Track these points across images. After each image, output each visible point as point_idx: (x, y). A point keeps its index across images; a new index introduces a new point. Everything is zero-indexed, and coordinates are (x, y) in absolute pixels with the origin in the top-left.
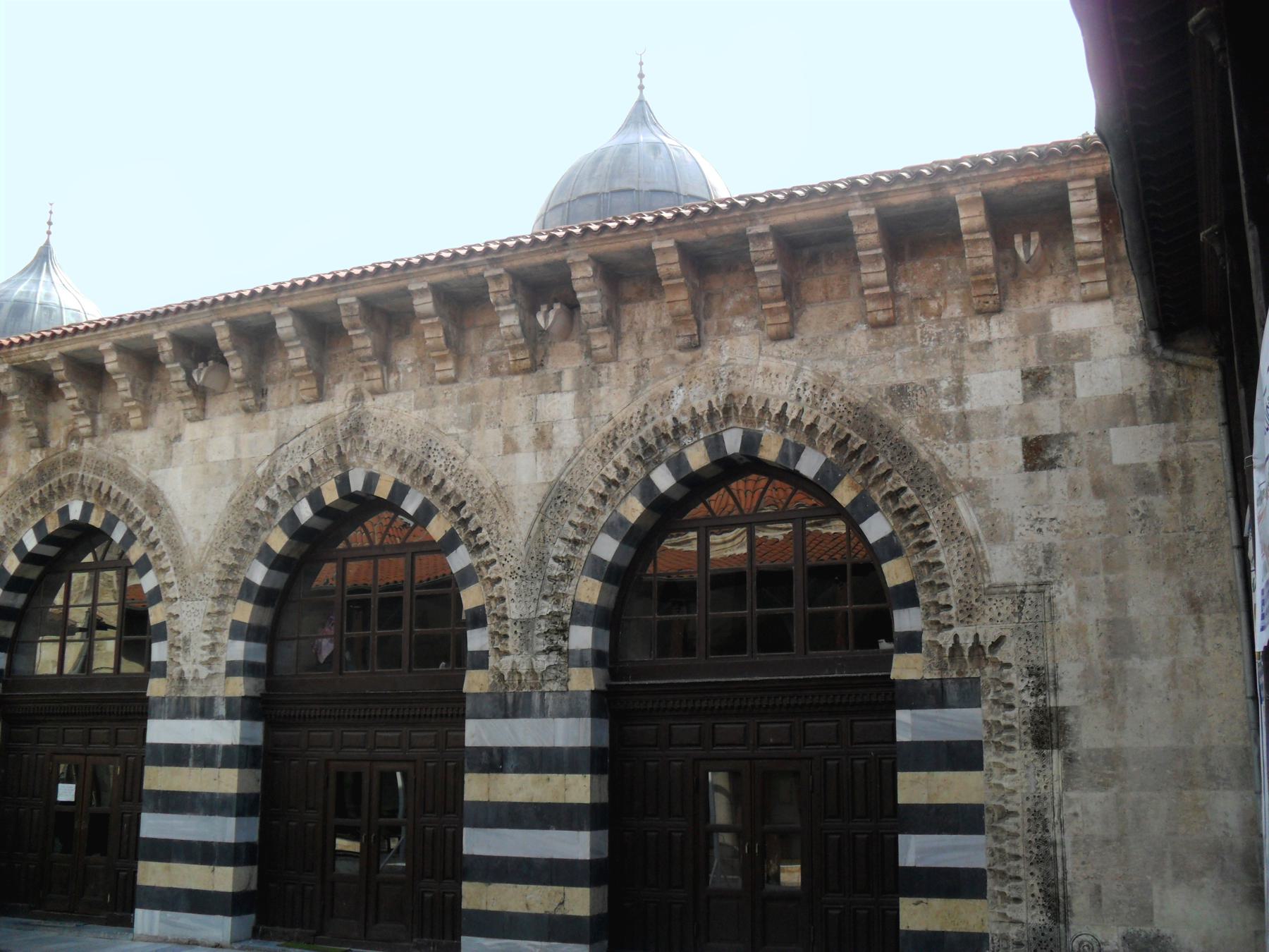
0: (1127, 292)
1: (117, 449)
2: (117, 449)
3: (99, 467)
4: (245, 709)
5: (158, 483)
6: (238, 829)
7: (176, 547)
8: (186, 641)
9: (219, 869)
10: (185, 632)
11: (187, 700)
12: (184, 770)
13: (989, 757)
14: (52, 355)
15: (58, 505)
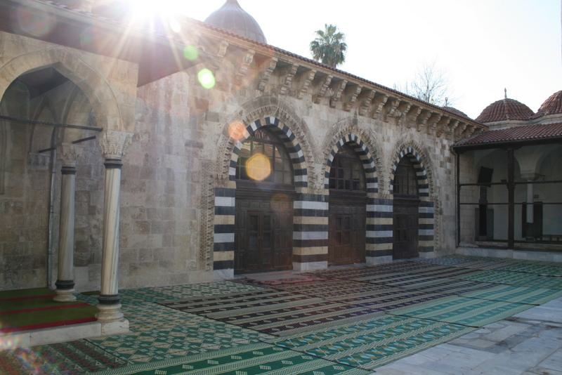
0: (154, 66)
1: (291, 103)
2: (291, 103)
3: (285, 107)
4: (327, 199)
5: (305, 120)
6: (301, 236)
7: (312, 146)
8: (317, 176)
9: (324, 247)
10: (316, 174)
11: (314, 195)
12: (314, 218)
13: (435, 216)
14: (296, 64)
15: (265, 116)
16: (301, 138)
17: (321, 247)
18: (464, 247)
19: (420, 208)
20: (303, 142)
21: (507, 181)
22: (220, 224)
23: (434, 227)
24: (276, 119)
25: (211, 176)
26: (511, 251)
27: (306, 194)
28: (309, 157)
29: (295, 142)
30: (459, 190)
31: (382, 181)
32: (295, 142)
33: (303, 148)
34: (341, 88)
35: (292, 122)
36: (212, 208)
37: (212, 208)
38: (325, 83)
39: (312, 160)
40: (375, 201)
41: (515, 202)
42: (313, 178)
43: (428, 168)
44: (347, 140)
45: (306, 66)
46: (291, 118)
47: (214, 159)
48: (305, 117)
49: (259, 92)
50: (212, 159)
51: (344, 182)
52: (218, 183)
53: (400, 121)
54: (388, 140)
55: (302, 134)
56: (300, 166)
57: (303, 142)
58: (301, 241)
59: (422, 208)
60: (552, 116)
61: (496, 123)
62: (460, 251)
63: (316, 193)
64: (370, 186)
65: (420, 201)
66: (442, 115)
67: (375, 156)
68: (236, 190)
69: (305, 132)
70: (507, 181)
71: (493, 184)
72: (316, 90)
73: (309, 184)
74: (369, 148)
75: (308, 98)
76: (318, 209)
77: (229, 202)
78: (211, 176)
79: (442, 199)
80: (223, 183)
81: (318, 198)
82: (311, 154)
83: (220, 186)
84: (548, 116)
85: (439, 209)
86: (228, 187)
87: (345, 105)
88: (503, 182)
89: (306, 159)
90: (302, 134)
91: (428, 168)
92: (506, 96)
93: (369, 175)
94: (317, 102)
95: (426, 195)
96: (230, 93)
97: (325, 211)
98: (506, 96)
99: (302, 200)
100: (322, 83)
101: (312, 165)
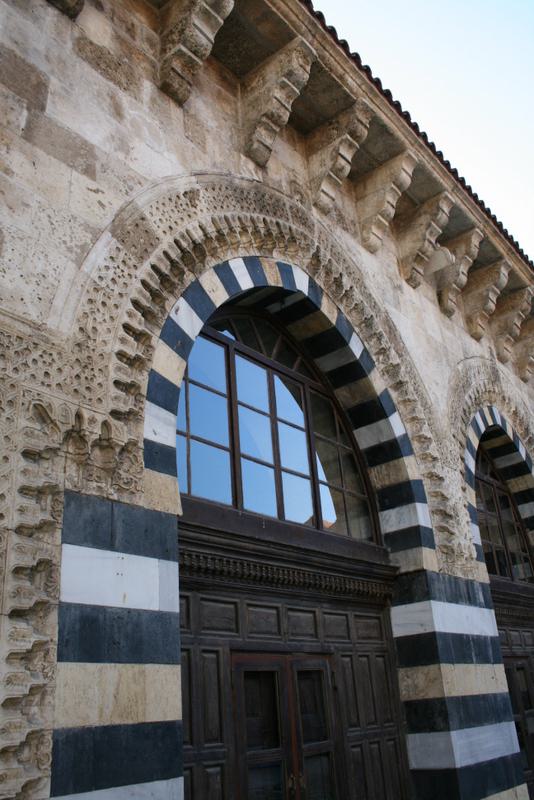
6: (450, 751)
8: (454, 508)
16: (392, 371)
22: (94, 720)
24: (312, 284)
25: (42, 414)
29: (378, 382)
33: (401, 407)
34: (468, 253)
36: (41, 607)
37: (41, 607)
39: (433, 450)
40: (437, 586)
42: (446, 515)
45: (399, 134)
46: (357, 295)
47: (63, 324)
49: (251, 166)
50: (51, 323)
52: (84, 463)
56: (400, 469)
63: (460, 575)
68: (182, 523)
69: (400, 356)
73: (438, 538)
76: (476, 632)
77: (144, 584)
78: (42, 414)
80: (112, 472)
81: (461, 593)
82: (426, 432)
83: (91, 489)
86: (141, 501)
87: (469, 320)
89: (416, 445)
90: (396, 360)
94: (412, 282)
96: (145, 108)
99: (427, 596)
100: (424, 219)
101: (438, 471)
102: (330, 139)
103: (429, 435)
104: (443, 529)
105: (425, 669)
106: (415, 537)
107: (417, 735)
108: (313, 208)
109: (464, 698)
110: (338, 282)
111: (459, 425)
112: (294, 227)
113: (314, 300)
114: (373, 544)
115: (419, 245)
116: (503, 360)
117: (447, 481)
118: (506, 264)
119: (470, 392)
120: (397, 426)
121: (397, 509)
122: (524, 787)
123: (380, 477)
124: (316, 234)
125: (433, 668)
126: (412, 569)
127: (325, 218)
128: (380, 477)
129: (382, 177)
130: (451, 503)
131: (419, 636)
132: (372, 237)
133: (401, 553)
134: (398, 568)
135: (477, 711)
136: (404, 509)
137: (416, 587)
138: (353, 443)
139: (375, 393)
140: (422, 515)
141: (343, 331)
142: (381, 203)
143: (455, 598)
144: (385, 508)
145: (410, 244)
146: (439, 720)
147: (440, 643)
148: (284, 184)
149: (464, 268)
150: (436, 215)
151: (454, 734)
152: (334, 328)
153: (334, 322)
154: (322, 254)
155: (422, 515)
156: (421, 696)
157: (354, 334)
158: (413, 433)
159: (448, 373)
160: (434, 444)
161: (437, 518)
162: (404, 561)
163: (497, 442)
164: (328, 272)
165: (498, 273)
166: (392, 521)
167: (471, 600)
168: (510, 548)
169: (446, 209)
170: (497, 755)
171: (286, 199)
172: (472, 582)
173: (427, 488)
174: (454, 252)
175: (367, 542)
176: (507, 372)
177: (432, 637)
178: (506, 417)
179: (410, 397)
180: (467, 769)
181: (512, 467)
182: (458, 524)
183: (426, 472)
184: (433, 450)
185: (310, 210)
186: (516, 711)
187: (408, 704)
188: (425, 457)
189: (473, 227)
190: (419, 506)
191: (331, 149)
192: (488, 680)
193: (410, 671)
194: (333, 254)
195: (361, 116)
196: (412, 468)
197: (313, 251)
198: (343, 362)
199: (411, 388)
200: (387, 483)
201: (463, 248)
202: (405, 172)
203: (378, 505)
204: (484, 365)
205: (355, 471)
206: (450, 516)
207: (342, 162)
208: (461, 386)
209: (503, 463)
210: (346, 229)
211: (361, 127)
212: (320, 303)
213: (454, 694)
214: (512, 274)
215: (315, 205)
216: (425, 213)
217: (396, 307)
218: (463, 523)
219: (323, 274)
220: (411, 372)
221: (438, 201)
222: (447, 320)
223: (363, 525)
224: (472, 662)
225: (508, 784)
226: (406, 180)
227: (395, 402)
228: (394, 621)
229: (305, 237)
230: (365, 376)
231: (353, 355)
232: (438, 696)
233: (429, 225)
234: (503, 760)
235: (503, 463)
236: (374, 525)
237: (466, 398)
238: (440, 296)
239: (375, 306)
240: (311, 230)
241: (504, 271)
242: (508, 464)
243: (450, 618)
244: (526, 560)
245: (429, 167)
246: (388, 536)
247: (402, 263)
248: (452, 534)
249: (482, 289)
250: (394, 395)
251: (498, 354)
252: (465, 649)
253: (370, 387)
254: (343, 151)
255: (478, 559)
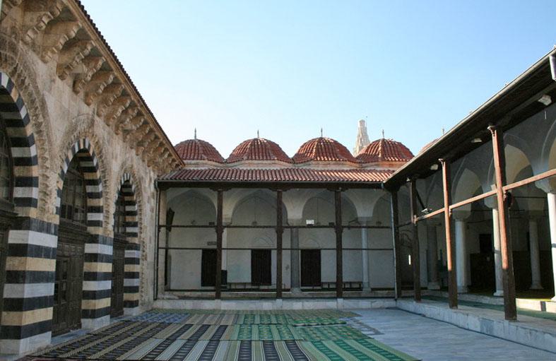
7: (50, 142)
8: (50, 191)
13: (141, 261)
16: (38, 125)
17: (45, 309)
18: (163, 299)
19: (126, 251)
20: (39, 132)
21: (216, 224)
23: (140, 275)
24: (10, 81)
26: (219, 301)
27: (35, 219)
28: (45, 159)
29: (30, 130)
30: (159, 231)
31: (108, 212)
32: (30, 130)
33: (38, 143)
34: (95, 67)
35: (30, 95)
38: (82, 50)
39: (48, 164)
41: (343, 247)
42: (45, 194)
43: (139, 202)
44: (82, 147)
46: (31, 88)
48: (47, 93)
51: (67, 207)
53: (128, 137)
54: (118, 158)
55: (41, 119)
56: (29, 171)
57: (39, 132)
58: (22, 299)
59: (129, 251)
60: (250, 161)
61: (193, 162)
62: (159, 304)
63: (45, 220)
64: (92, 217)
65: (127, 242)
66: (161, 140)
67: (104, 177)
69: (44, 117)
70: (216, 224)
71: (174, 226)
72: (66, 59)
73: (39, 203)
74: (100, 164)
75: (53, 65)
76: (46, 245)
79: (147, 241)
81: (44, 228)
84: (247, 162)
85: (144, 253)
87: (87, 95)
88: (331, 225)
89: (40, 161)
90: (41, 119)
91: (139, 202)
92: (195, 137)
93: (92, 202)
94: (62, 77)
95: (135, 235)
97: (54, 249)
98: (195, 137)
99: (28, 228)
100: (77, 49)
101: (47, 174)
102: (39, 9)
103: (47, 157)
104: (42, 200)
105: (20, 258)
106: (29, 202)
107: (10, 285)
108: (20, 42)
109: (34, 272)
110: (23, 82)
111: (64, 151)
112: (8, 54)
113: (8, 90)
114: (8, 201)
115: (70, 61)
116: (99, 115)
117: (51, 178)
118: (113, 74)
119: (75, 134)
120: (33, 151)
121: (24, 188)
122: (52, 308)
123: (19, 171)
124: (18, 57)
125: (23, 258)
126: (24, 216)
127: (25, 47)
128: (19, 171)
129: (61, 27)
130: (49, 189)
131: (20, 244)
132: (47, 57)
133: (20, 208)
134: (17, 214)
135: (39, 277)
136: (27, 189)
137: (23, 224)
138: (9, 153)
139: (26, 136)
140: (35, 193)
141: (19, 106)
142: (56, 42)
143: (40, 230)
144: (17, 186)
145: (66, 59)
146: (21, 279)
147: (29, 249)
148: (8, 29)
149: (90, 74)
150: (84, 50)
151: (26, 285)
152: (15, 104)
153: (15, 101)
154: (18, 68)
155: (35, 193)
156: (16, 269)
157: (24, 107)
158: (40, 155)
159: (66, 124)
160: (49, 161)
161: (41, 194)
162: (21, 212)
163: (84, 155)
164: (19, 76)
165: (109, 77)
166: (19, 192)
167: (48, 231)
168: (76, 204)
169: (89, 48)
170: (43, 295)
171: (7, 39)
172: (50, 223)
173: (40, 181)
174: (88, 66)
175: (4, 200)
176: (99, 122)
177: (26, 246)
178: (91, 144)
179: (43, 138)
180: (29, 299)
181: (89, 167)
182: (50, 198)
183: (41, 173)
184: (48, 164)
185: (19, 42)
186: (57, 279)
187: (9, 272)
188: (43, 167)
189: (101, 56)
190: (34, 188)
191: (38, 15)
192: (49, 265)
193: (13, 258)
194: (24, 67)
195: (58, 5)
196: (35, 171)
197: (15, 66)
198: (15, 118)
199: (45, 134)
200: (21, 175)
201: (93, 64)
202: (73, 32)
203: (14, 183)
204: (88, 118)
205: (7, 165)
206: (48, 195)
207: (42, 24)
208: (72, 129)
209: (83, 164)
210: (34, 51)
211: (57, 11)
212: (11, 91)
213: (30, 270)
214: (115, 78)
215: (22, 40)
216: (79, 46)
217: (49, 92)
218: (53, 198)
219: (16, 77)
220: (48, 126)
221: (86, 43)
222: (75, 96)
223: (4, 191)
224: (41, 257)
225: (46, 306)
226: (73, 35)
227: (35, 139)
228: (10, 237)
229: (12, 58)
230: (24, 127)
231: (21, 117)
232: (23, 269)
233: (79, 54)
234: (46, 297)
235: (83, 164)
236: (11, 193)
237: (72, 137)
238: (74, 83)
239: (38, 92)
240: (16, 54)
241: (112, 77)
242: (87, 165)
243: (35, 238)
244: (83, 212)
245: (87, 29)
246: (16, 199)
247: (59, 66)
248: (46, 202)
249: (98, 82)
250: (36, 136)
251: (97, 112)
252: (39, 252)
253: (25, 132)
254: (44, 19)
255: (56, 213)
